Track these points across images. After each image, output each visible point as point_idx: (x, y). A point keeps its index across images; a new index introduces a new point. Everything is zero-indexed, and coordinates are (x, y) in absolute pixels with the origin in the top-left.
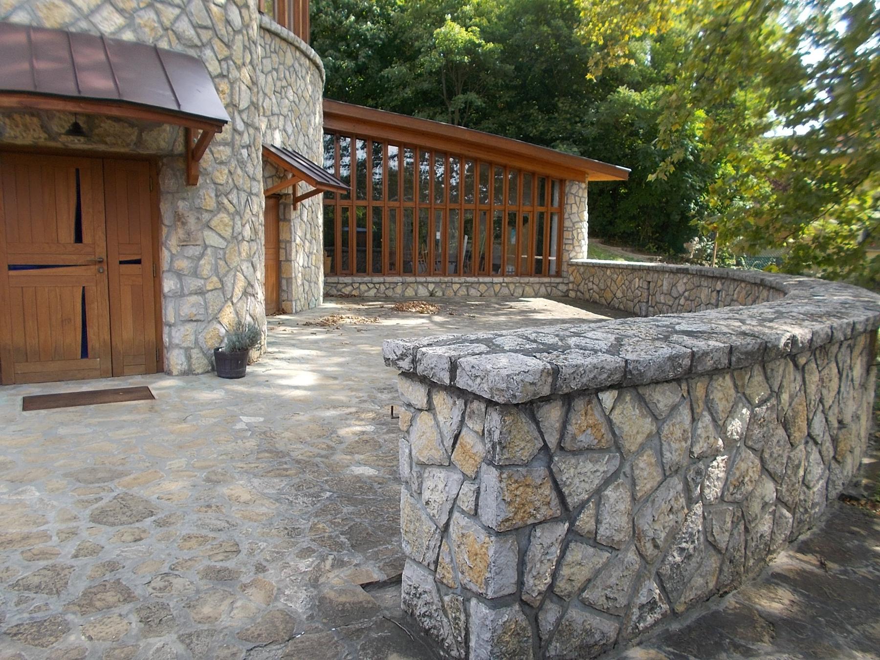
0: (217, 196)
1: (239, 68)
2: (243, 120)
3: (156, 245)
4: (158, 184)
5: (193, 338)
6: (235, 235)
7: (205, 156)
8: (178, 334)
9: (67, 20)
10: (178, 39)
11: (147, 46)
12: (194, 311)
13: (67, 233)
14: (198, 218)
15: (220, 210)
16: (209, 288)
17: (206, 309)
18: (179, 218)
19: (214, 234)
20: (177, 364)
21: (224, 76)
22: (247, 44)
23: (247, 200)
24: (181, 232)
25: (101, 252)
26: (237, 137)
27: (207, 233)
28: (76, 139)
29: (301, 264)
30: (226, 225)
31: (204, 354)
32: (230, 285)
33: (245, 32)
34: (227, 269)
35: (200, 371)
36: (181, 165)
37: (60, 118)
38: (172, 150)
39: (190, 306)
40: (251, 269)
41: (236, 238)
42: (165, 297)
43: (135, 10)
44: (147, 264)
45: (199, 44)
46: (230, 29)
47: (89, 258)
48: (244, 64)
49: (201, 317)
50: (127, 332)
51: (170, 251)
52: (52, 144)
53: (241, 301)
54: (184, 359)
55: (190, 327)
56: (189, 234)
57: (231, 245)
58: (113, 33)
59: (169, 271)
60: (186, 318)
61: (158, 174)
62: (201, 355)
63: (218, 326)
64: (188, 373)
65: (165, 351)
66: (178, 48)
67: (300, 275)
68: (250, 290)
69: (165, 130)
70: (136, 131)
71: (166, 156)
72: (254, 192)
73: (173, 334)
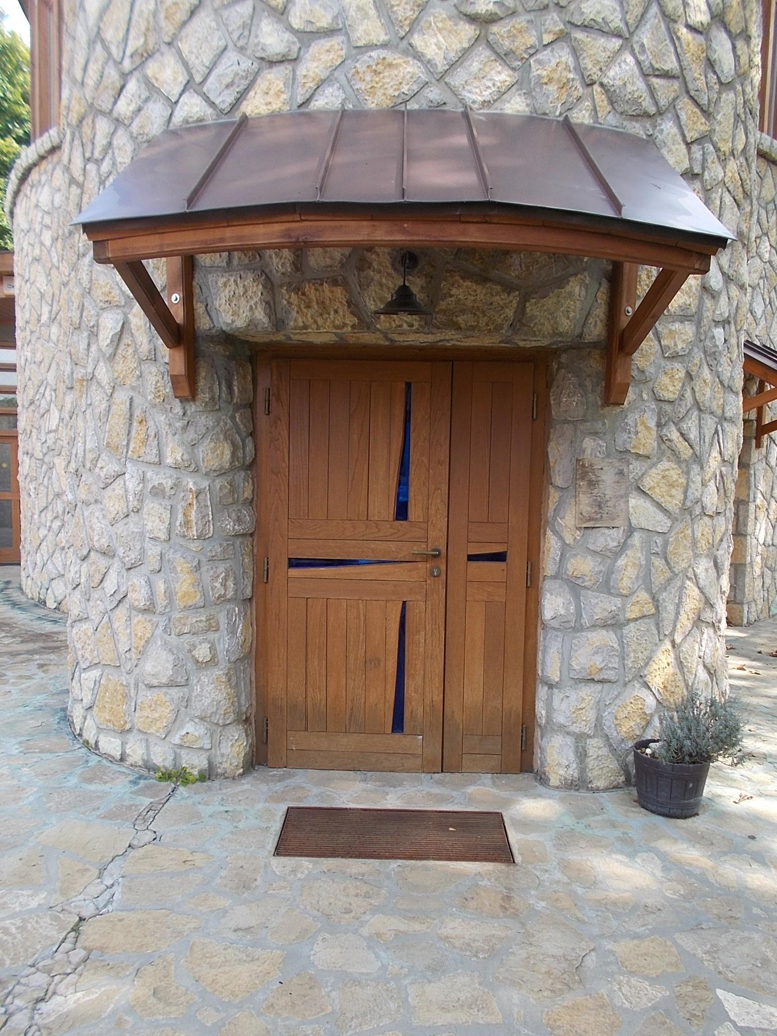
0: (659, 425)
1: (723, 160)
2: (721, 269)
3: (535, 525)
4: (548, 406)
5: (591, 715)
6: (689, 504)
7: (644, 344)
8: (564, 706)
9: (405, 89)
10: (611, 102)
11: (550, 122)
12: (598, 661)
13: (382, 505)
14: (621, 473)
15: (663, 453)
16: (630, 615)
17: (623, 658)
18: (584, 473)
19: (648, 504)
20: (559, 764)
21: (695, 176)
22: (741, 111)
23: (716, 432)
24: (585, 503)
25: (437, 537)
26: (708, 303)
27: (635, 501)
28: (403, 320)
29: (761, 541)
30: (672, 485)
31: (613, 750)
32: (671, 608)
33: (739, 88)
34: (668, 574)
35: (601, 784)
36: (594, 364)
37: (381, 284)
38: (580, 336)
39: (591, 650)
40: (713, 573)
41: (690, 511)
42: (545, 627)
43: (533, 51)
44: (514, 562)
45: (652, 110)
46: (713, 78)
47: (416, 549)
48: (732, 154)
49: (609, 675)
50: (473, 690)
51: (561, 538)
52: (368, 338)
53: (690, 639)
54: (572, 757)
55: (588, 693)
56: (600, 505)
57: (679, 526)
58: (486, 104)
59: (555, 577)
60: (584, 675)
61: (548, 386)
62: (605, 751)
63: (644, 693)
64: (578, 784)
65: (538, 732)
66: (611, 120)
67: (758, 559)
68: (708, 616)
69: (570, 294)
70: (514, 300)
71: (566, 349)
72: (728, 414)
73: (556, 703)
